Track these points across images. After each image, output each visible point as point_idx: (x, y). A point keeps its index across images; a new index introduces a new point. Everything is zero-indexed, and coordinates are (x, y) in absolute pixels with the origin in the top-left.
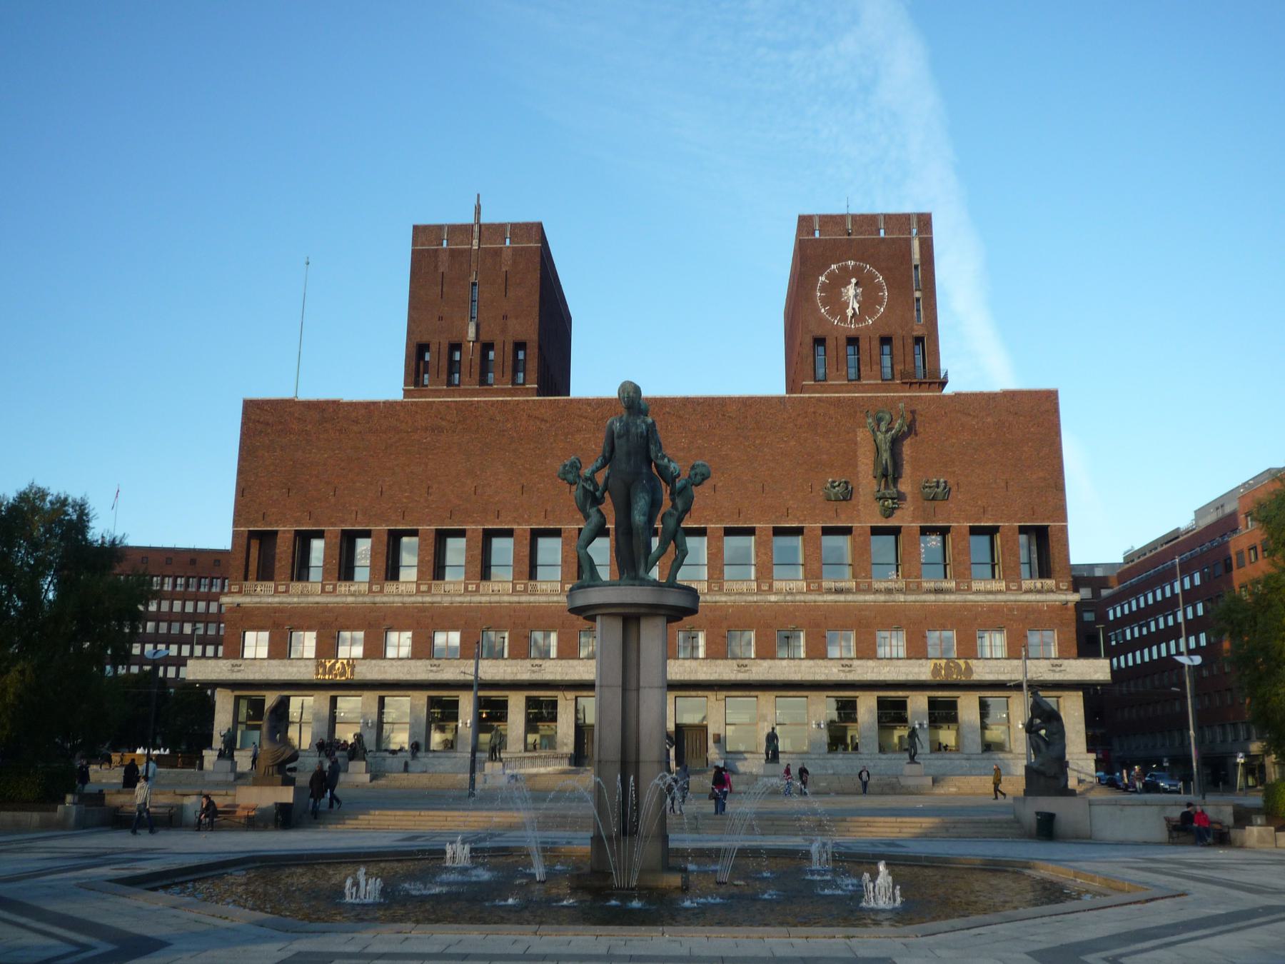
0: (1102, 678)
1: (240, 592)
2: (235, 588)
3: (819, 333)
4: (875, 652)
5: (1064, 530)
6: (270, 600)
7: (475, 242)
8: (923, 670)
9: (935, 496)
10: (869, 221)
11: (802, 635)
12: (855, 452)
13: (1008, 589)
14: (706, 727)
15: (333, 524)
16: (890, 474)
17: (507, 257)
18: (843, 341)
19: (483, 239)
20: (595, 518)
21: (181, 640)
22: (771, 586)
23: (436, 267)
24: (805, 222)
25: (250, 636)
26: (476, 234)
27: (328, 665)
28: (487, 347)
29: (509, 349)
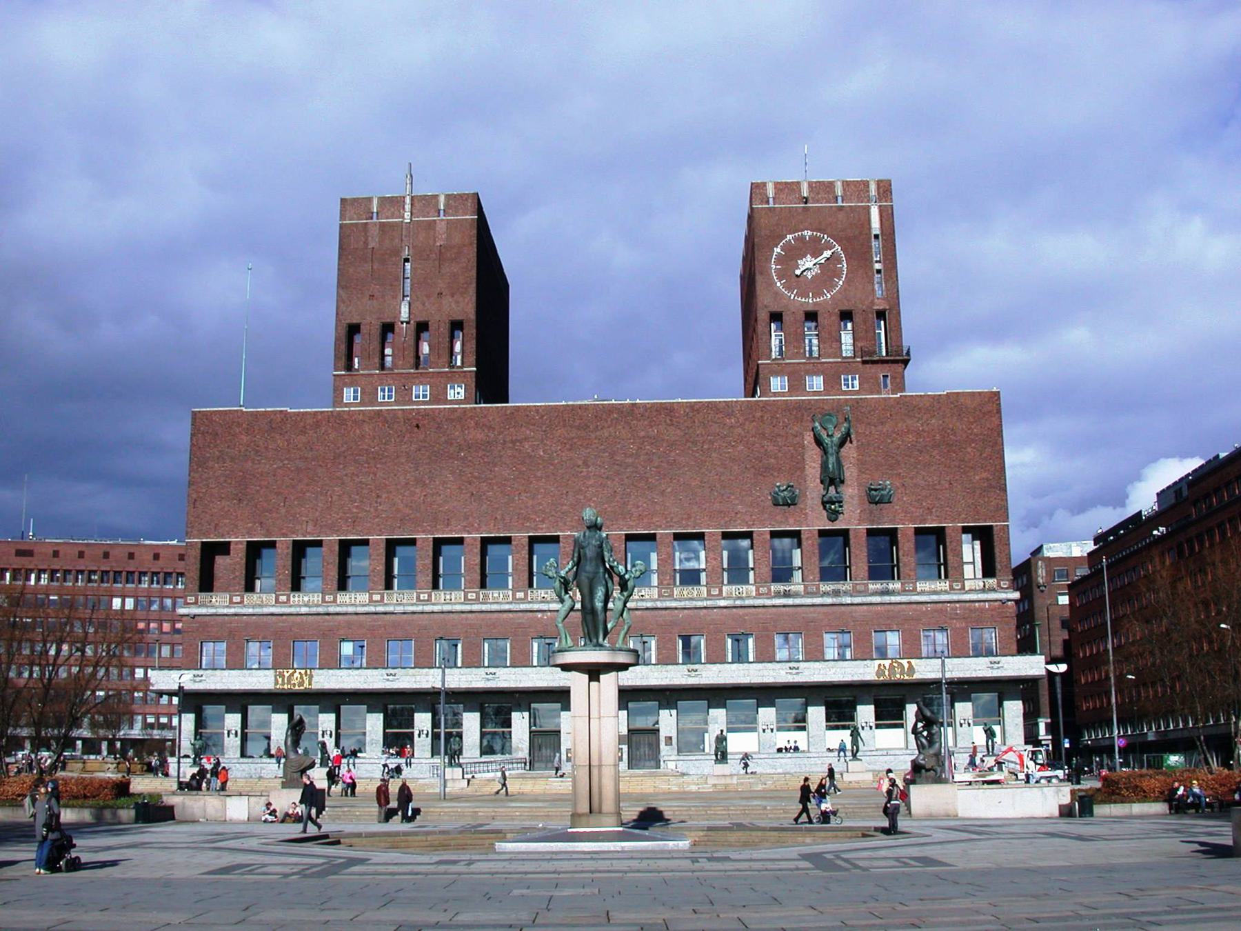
1: (196, 603)
2: (191, 599)
4: (823, 653)
6: (226, 611)
7: (407, 215)
8: (868, 670)
11: (751, 641)
13: (951, 588)
15: (284, 535)
16: (832, 479)
17: (441, 228)
20: (568, 603)
23: (366, 243)
26: (408, 207)
27: (287, 675)
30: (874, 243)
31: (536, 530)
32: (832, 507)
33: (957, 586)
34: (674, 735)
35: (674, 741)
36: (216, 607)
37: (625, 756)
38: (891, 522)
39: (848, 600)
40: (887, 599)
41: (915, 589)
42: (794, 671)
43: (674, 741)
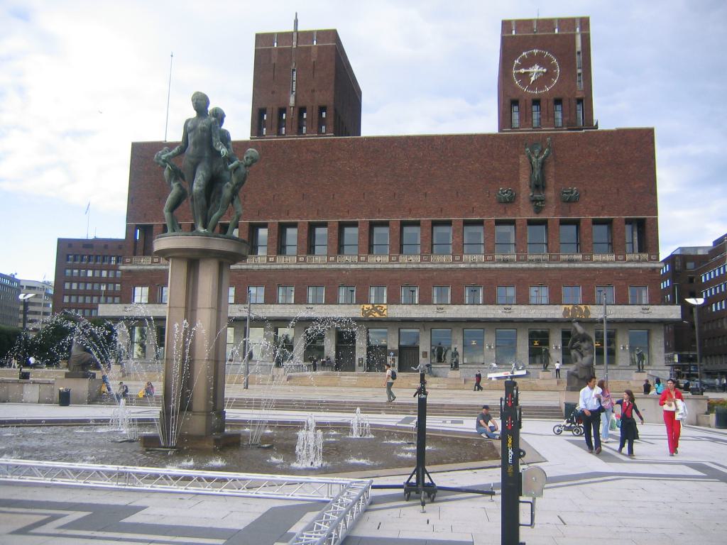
0: (675, 317)
1: (131, 262)
2: (128, 260)
3: (514, 97)
5: (655, 221)
6: (149, 267)
7: (294, 43)
8: (557, 312)
9: (569, 200)
10: (547, 24)
12: (518, 170)
13: (617, 259)
14: (418, 347)
15: (186, 220)
16: (539, 186)
17: (314, 52)
18: (530, 102)
19: (299, 41)
21: (92, 294)
22: (461, 258)
23: (270, 60)
24: (506, 25)
25: (138, 290)
26: (295, 38)
28: (302, 110)
29: (316, 111)
30: (577, 56)
31: (343, 217)
32: (538, 205)
33: (620, 257)
34: (428, 351)
35: (429, 355)
36: (144, 265)
37: (396, 364)
38: (576, 214)
39: (546, 266)
40: (572, 265)
41: (591, 259)
42: (508, 311)
43: (429, 355)
